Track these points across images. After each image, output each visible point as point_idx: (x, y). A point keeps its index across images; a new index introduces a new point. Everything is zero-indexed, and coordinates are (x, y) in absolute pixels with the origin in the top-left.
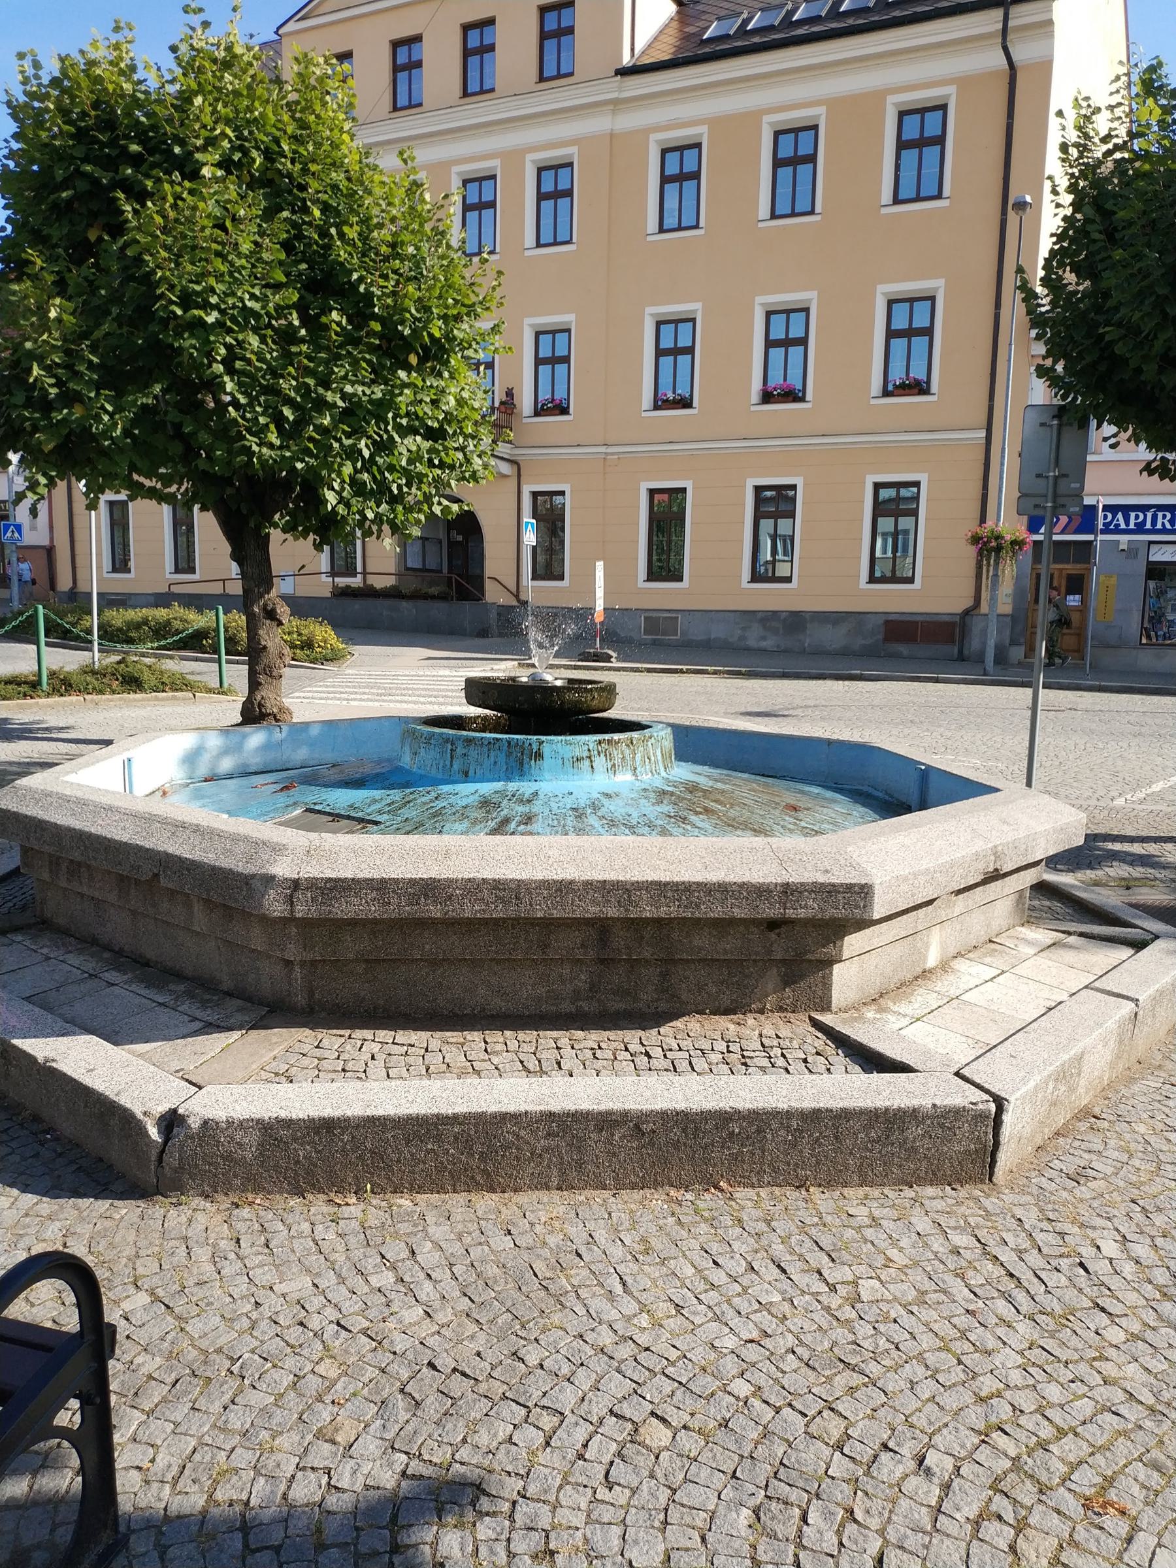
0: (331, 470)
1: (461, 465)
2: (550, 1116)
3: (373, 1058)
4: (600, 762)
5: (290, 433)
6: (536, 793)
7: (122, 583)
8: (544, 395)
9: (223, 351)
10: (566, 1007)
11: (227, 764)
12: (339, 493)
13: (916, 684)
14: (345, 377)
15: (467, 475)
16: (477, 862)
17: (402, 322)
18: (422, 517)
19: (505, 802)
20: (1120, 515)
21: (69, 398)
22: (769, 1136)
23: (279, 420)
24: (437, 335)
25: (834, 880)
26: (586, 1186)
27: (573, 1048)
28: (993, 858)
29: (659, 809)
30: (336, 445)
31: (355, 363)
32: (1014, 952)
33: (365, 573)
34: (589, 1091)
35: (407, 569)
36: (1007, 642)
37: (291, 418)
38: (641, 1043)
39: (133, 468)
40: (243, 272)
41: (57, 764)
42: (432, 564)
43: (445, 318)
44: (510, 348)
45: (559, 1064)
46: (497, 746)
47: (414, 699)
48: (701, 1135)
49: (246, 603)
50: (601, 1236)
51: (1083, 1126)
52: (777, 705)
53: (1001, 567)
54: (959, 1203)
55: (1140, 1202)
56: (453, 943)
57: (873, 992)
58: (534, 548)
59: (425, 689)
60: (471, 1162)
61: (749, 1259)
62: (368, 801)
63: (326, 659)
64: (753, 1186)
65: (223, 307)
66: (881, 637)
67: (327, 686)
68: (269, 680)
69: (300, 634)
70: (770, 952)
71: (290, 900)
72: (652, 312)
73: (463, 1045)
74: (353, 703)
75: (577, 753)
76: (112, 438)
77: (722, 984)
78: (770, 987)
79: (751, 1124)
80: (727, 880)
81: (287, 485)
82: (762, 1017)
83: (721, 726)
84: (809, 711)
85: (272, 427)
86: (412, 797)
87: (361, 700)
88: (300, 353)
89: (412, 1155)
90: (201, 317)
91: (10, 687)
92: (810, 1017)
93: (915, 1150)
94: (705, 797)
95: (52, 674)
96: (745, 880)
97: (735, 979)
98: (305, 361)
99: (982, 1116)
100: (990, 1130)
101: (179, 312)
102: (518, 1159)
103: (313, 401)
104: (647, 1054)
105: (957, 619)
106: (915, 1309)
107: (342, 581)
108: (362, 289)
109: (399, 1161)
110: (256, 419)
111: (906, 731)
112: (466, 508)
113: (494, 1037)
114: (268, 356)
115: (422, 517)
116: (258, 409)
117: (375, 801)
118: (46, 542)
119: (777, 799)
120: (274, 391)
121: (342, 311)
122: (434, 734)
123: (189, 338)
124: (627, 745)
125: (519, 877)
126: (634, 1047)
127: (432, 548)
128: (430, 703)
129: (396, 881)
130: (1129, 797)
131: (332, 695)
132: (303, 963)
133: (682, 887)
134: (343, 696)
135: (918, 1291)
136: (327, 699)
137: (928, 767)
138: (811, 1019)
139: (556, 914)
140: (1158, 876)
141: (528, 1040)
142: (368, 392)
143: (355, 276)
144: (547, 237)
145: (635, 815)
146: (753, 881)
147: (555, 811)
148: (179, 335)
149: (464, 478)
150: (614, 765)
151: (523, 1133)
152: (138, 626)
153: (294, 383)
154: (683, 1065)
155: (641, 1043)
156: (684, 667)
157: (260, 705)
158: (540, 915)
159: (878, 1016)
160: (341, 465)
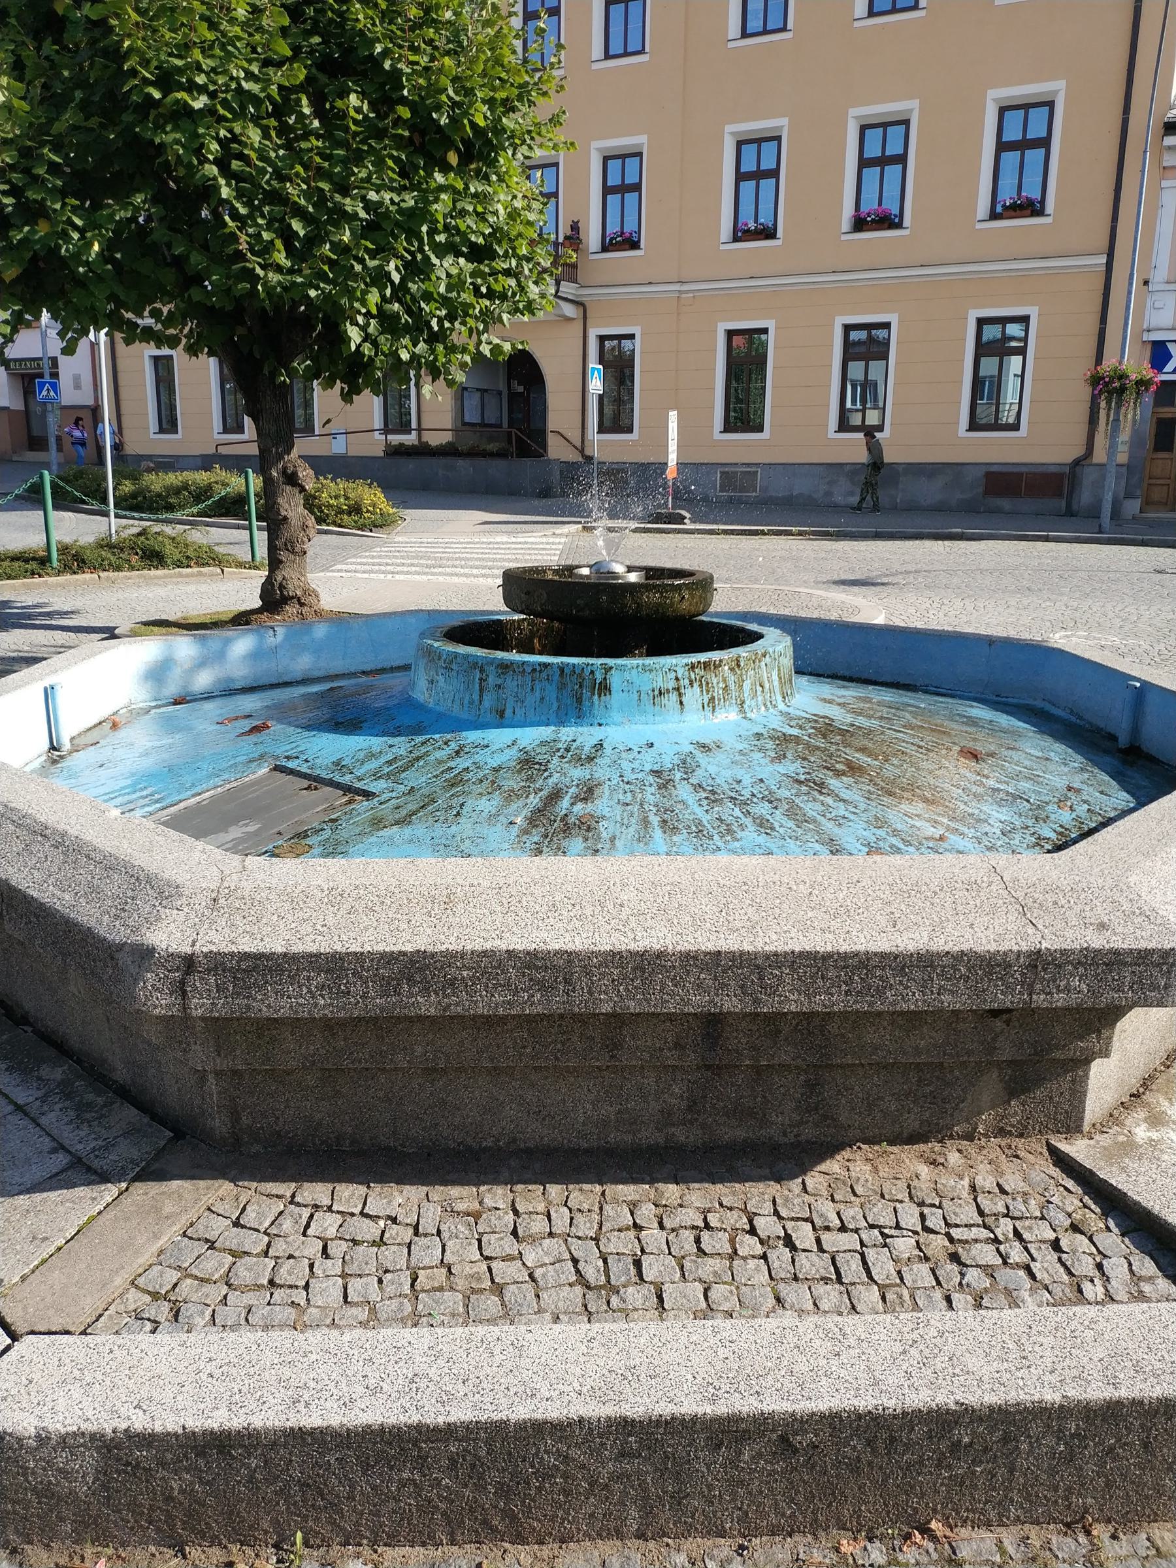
0: (352, 298)
1: (514, 295)
2: (625, 1425)
3: (325, 1252)
4: (693, 696)
5: (300, 251)
6: (600, 746)
7: (167, 444)
8: (613, 228)
9: (214, 146)
10: (649, 1135)
11: (204, 680)
12: (364, 328)
13: (1023, 543)
14: (368, 179)
15: (521, 305)
16: (499, 918)
17: (438, 107)
18: (467, 359)
19: (556, 760)
21: (32, 212)
22: (1024, 1447)
23: (288, 236)
24: (482, 123)
25: (1118, 943)
26: (688, 1532)
27: (662, 1227)
29: (781, 768)
30: (358, 268)
31: (380, 163)
33: (420, 430)
34: (697, 1360)
35: (465, 424)
36: (1122, 495)
37: (302, 233)
38: (776, 1213)
39: (120, 304)
40: (238, 44)
41: (45, 659)
42: (491, 418)
43: (490, 102)
44: (572, 144)
45: (638, 1264)
46: (544, 675)
47: (466, 571)
48: (900, 1449)
49: (263, 464)
56: (461, 1043)
57: (1134, 1084)
58: (601, 398)
59: (480, 559)
60: (481, 1498)
62: (362, 755)
63: (375, 526)
64: (988, 1524)
65: (212, 88)
66: (981, 490)
67: (373, 557)
68: (292, 557)
69: (347, 498)
70: (991, 1050)
71: (181, 990)
72: (733, 130)
73: (477, 1216)
74: (397, 577)
75: (660, 684)
76: (87, 263)
77: (907, 1096)
78: (986, 1098)
79: (992, 1429)
80: (934, 948)
81: (306, 323)
82: (970, 1148)
84: (911, 579)
85: (279, 244)
86: (423, 750)
87: (408, 573)
88: (311, 150)
89: (375, 1488)
90: (186, 103)
91: (16, 564)
92: (1048, 1145)
95: (64, 549)
97: (928, 1089)
98: (318, 159)
101: (157, 95)
102: (566, 1493)
103: (330, 212)
104: (789, 1242)
105: (1067, 470)
107: (395, 439)
108: (387, 65)
109: (351, 1498)
110: (259, 234)
111: (1026, 601)
112: (520, 347)
113: (531, 1198)
114: (273, 155)
115: (467, 359)
116: (260, 221)
117: (371, 756)
118: (90, 402)
120: (277, 198)
121: (363, 95)
122: (456, 655)
123: (172, 131)
124: (732, 669)
125: (570, 947)
126: (767, 1225)
127: (491, 402)
128: (483, 576)
129: (359, 957)
131: (377, 568)
132: (218, 1074)
133: (855, 962)
134: (389, 568)
136: (372, 572)
137: (1145, 684)
138: (1053, 1151)
139: (633, 1007)
141: (586, 1206)
142: (397, 199)
143: (378, 49)
144: (616, 47)
145: (747, 781)
146: (979, 949)
147: (629, 776)
148: (159, 128)
149: (517, 310)
150: (713, 698)
151: (575, 1453)
152: (177, 491)
153: (304, 187)
154: (852, 1268)
155: (776, 1213)
156: (765, 528)
157: (282, 587)
158: (606, 1008)
159: (1155, 1135)
160: (365, 292)
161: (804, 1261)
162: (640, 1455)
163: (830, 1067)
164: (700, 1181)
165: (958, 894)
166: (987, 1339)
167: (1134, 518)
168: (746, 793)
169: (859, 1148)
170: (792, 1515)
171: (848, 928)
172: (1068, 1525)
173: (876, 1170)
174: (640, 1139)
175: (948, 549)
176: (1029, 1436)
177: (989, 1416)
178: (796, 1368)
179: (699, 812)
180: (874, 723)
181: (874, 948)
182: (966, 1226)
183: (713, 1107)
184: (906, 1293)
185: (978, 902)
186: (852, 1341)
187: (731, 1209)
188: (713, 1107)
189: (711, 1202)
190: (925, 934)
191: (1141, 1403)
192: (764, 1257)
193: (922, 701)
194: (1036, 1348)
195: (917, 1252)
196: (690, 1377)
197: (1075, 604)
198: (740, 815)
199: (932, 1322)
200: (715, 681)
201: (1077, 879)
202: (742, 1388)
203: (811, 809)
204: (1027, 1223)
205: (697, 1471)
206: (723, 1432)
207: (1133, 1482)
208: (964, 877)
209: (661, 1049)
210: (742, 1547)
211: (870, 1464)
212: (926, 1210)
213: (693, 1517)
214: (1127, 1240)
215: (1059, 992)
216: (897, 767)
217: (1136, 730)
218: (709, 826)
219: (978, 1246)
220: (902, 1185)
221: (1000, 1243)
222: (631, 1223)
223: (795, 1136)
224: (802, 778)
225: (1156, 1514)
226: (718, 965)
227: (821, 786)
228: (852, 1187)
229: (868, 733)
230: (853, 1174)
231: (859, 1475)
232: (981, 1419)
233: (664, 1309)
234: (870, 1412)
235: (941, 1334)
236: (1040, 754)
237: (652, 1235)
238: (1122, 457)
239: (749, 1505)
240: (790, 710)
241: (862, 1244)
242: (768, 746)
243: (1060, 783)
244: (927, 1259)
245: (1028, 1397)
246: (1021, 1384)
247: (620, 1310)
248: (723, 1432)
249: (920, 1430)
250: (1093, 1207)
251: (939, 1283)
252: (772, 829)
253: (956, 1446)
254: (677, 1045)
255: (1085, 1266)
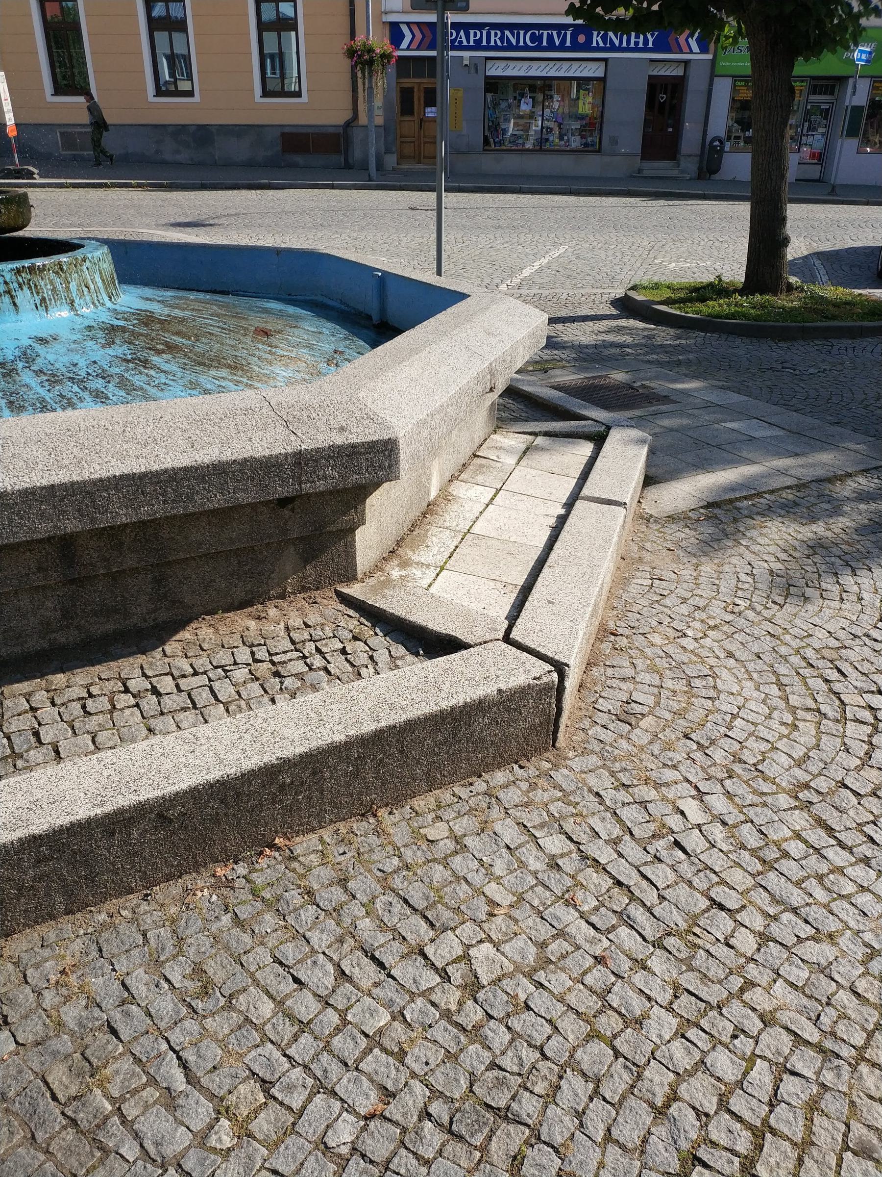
2: (35, 840)
4: (24, 297)
10: (34, 644)
13: (316, 190)
20: (462, 33)
26: (105, 898)
27: (53, 704)
28: (489, 377)
29: (111, 351)
32: (499, 465)
34: (86, 783)
38: (144, 675)
45: (36, 734)
48: (245, 799)
50: (139, 981)
51: (606, 647)
52: (203, 214)
53: (374, 80)
54: (533, 787)
55: (693, 736)
57: (391, 545)
61: (335, 958)
64: (313, 830)
66: (279, 148)
77: (232, 575)
80: (224, 458)
82: (283, 604)
83: (155, 239)
92: (336, 590)
93: (482, 740)
94: (164, 330)
96: (247, 455)
97: (247, 568)
99: (546, 689)
100: (553, 701)
104: (155, 691)
106: (541, 976)
111: (320, 234)
119: (244, 324)
124: (56, 273)
126: (137, 684)
130: (508, 282)
135: (536, 943)
138: (339, 594)
140: (563, 356)
145: (82, 363)
146: (257, 455)
150: (43, 300)
154: (202, 698)
155: (144, 675)
159: (404, 573)
161: (168, 701)
162: (53, 858)
163: (169, 563)
164: (83, 666)
165: (238, 418)
166: (296, 716)
167: (394, 169)
168: (83, 374)
169: (204, 619)
170: (179, 864)
171: (156, 453)
172: (363, 815)
173: (217, 631)
174: (28, 648)
175: (260, 196)
176: (329, 767)
177: (301, 761)
178: (163, 768)
179: (42, 392)
180: (187, 314)
181: (178, 464)
182: (283, 653)
183: (83, 611)
184: (243, 703)
185: (254, 422)
186: (203, 741)
187: (108, 680)
188: (83, 611)
189: (92, 678)
190: (216, 450)
191: (395, 727)
192: (137, 705)
193: (229, 299)
194: (329, 713)
195: (250, 676)
196: (82, 795)
197: (355, 235)
198: (79, 391)
199: (259, 715)
200: (42, 283)
201: (323, 398)
202: (123, 791)
203: (138, 380)
204: (324, 642)
205: (101, 855)
206: (113, 824)
207: (398, 777)
208: (242, 406)
209: (27, 575)
210: (147, 895)
211: (226, 814)
212: (254, 649)
213: (106, 887)
214: (387, 638)
215: (319, 479)
216: (206, 344)
217: (383, 310)
218: (52, 402)
219: (292, 663)
220: (237, 636)
221: (307, 658)
222: (28, 707)
223: (154, 620)
224: (129, 357)
225: (414, 793)
226: (55, 496)
227: (145, 363)
228: (200, 646)
229: (183, 320)
230: (201, 637)
231: (220, 824)
232: (295, 765)
233: (61, 758)
234: (218, 781)
235: (265, 720)
236: (315, 330)
237: (46, 712)
238: (379, 120)
239: (145, 867)
240: (117, 307)
241: (210, 680)
242: (99, 336)
243: (328, 348)
244: (257, 679)
245: (324, 743)
246: (319, 735)
247: (25, 768)
248: (113, 824)
249: (256, 783)
250: (366, 623)
251: (266, 692)
252: (107, 398)
253: (282, 787)
254: (40, 569)
255: (363, 659)
